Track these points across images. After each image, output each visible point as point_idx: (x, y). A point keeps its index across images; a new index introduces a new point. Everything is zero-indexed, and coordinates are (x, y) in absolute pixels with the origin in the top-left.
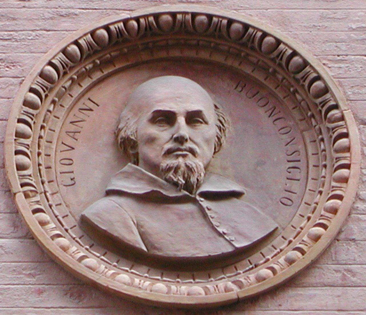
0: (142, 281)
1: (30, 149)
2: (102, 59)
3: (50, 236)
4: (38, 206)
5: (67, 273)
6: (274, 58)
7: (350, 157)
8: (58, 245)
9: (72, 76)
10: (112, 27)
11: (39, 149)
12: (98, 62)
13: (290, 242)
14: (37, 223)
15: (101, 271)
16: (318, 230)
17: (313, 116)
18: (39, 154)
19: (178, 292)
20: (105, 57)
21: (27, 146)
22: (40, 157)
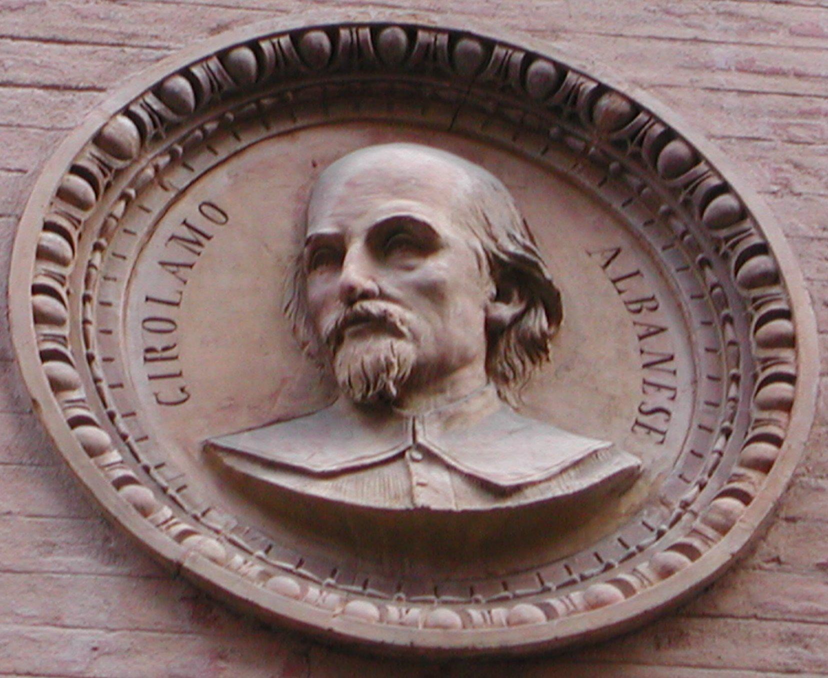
0: (404, 610)
1: (68, 285)
3: (111, 480)
5: (155, 562)
9: (172, 145)
11: (87, 287)
12: (230, 116)
14: (80, 447)
20: (246, 109)
22: (88, 305)
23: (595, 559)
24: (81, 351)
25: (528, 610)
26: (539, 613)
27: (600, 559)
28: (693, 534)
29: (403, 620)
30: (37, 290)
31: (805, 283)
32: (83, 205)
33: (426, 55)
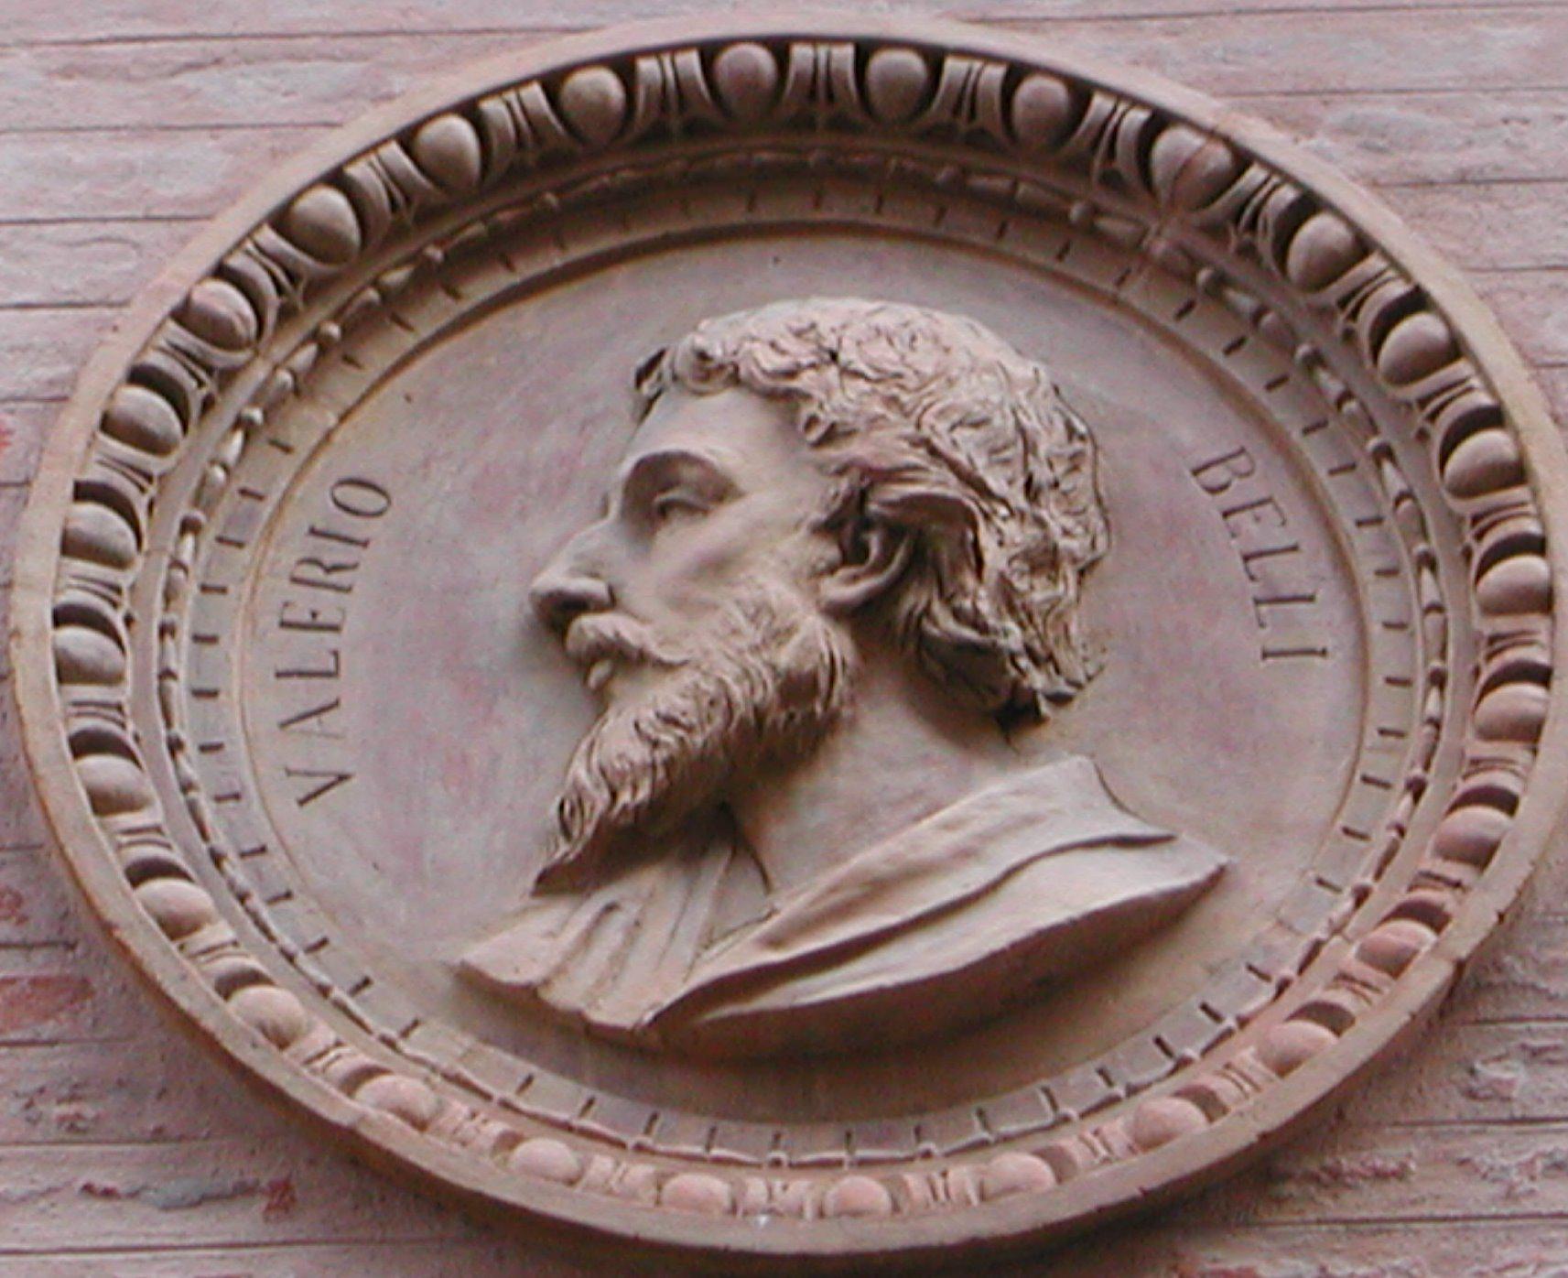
0: (778, 1184)
6: (1409, 405)
10: (492, 107)
12: (436, 253)
18: (175, 746)
21: (114, 713)
22: (181, 758)
23: (1157, 1050)
24: (158, 735)
25: (1018, 1164)
26: (1044, 1171)
27: (1167, 1051)
28: (1341, 982)
29: (775, 1204)
32: (152, 443)
33: (812, 93)
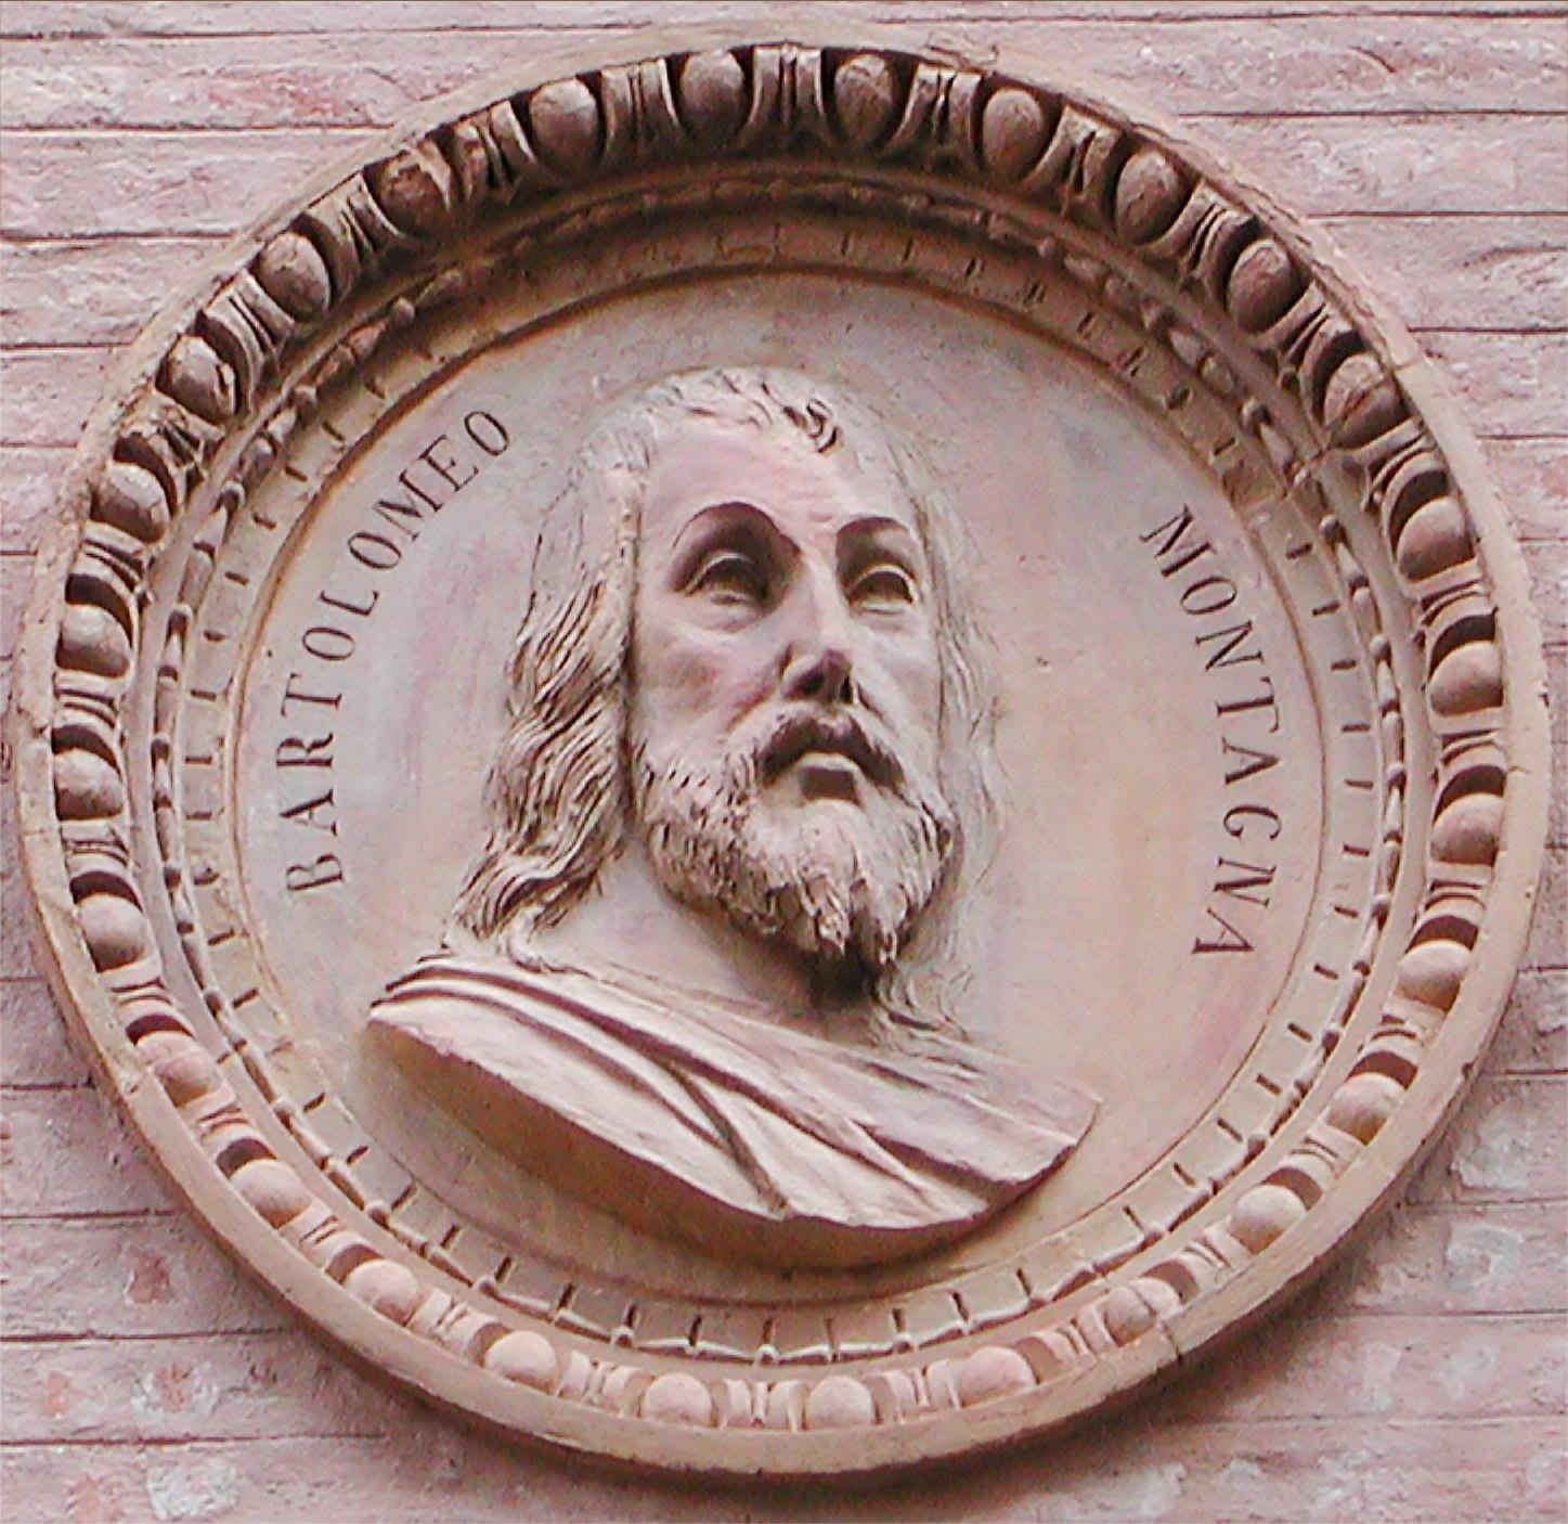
0: (762, 1386)
2: (320, 380)
4: (235, 1133)
7: (1486, 579)
8: (367, 1299)
13: (1330, 1042)
15: (582, 1387)
16: (1437, 953)
17: (1264, 416)
18: (172, 879)
19: (924, 1401)
30: (63, 741)
31: (1517, 546)
32: (139, 524)
